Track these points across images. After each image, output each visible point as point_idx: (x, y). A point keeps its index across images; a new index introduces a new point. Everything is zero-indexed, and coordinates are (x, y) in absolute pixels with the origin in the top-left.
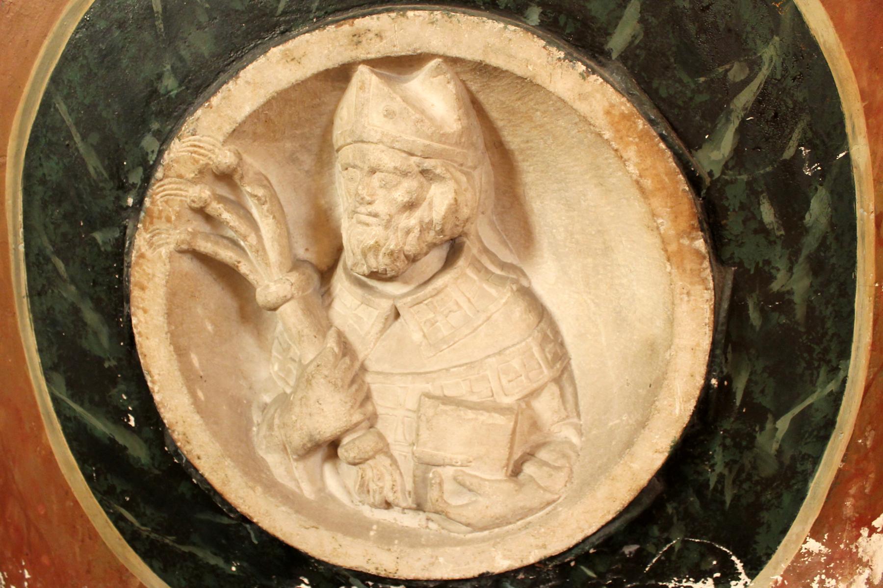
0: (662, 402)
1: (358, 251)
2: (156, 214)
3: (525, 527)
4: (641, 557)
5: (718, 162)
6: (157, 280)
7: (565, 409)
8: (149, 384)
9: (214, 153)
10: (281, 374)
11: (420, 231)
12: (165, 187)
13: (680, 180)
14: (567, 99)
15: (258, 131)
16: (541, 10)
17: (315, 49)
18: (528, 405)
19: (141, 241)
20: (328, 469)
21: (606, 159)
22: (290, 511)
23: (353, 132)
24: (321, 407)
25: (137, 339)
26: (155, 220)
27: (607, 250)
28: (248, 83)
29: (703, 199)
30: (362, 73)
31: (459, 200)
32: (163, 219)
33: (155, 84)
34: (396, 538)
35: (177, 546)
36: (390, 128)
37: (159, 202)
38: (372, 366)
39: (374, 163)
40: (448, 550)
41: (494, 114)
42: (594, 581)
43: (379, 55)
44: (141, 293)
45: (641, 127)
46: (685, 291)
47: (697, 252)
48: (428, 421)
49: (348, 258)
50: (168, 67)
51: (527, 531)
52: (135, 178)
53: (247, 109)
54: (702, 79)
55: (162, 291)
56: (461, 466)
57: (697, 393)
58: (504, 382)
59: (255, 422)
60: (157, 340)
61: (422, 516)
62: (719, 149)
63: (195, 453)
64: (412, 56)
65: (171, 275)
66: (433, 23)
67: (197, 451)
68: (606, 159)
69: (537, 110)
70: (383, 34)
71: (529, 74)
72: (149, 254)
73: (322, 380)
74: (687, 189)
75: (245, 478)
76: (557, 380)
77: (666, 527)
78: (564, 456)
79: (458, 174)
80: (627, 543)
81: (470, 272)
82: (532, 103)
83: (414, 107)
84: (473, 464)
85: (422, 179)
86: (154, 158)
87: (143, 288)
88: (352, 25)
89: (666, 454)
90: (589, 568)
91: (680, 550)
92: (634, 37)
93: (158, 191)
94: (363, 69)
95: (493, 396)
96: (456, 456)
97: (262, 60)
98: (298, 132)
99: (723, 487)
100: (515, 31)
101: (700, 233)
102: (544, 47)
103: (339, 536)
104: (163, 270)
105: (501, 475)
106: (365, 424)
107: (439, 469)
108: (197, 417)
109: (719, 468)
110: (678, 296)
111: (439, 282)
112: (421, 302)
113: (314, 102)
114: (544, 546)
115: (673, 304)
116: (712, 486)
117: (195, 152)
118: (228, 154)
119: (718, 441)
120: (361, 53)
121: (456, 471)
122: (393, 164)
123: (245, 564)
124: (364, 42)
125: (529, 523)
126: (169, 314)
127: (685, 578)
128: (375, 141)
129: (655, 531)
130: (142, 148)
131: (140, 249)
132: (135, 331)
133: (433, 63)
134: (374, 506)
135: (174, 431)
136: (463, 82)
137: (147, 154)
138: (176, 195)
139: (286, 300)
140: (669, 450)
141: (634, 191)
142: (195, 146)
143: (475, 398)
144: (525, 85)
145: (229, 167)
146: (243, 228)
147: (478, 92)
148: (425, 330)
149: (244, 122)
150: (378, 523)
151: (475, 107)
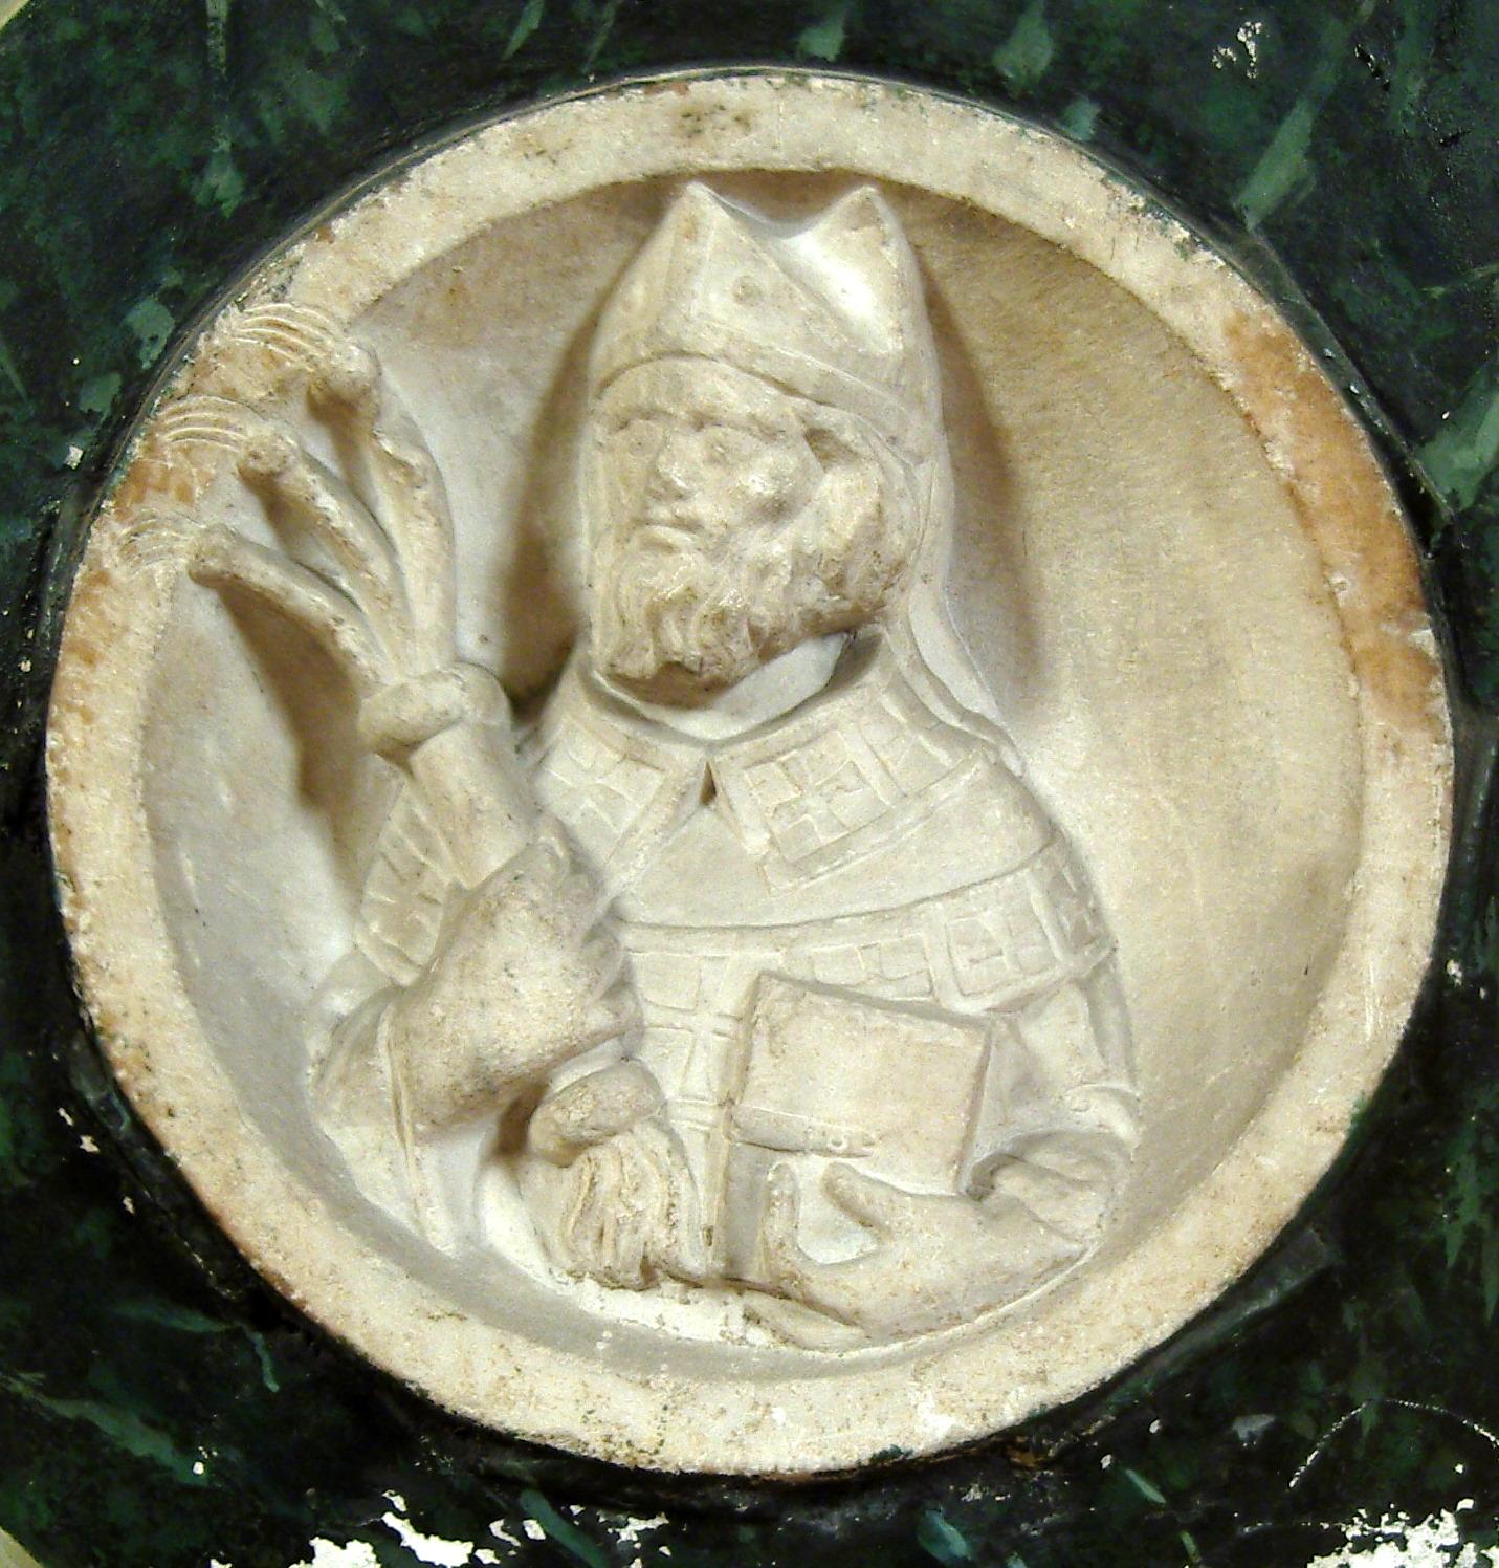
0: (1336, 1003)
1: (636, 615)
2: (156, 476)
3: (998, 1326)
4: (1279, 1450)
5: (1467, 474)
6: (131, 640)
7: (1103, 1054)
8: (66, 911)
9: (321, 348)
10: (389, 941)
11: (792, 573)
12: (189, 415)
13: (1384, 490)
14: (1145, 297)
15: (430, 312)
16: (1097, 110)
17: (598, 134)
18: (1013, 1027)
19: (106, 539)
20: (494, 1187)
21: (1226, 439)
22: (393, 1268)
23: (656, 331)
24: (513, 983)
25: (54, 787)
26: (150, 493)
27: (1216, 668)
28: (428, 194)
29: (1436, 555)
30: (693, 199)
31: (888, 511)
32: (172, 494)
33: (184, 182)
34: (665, 1361)
35: (46, 1402)
36: (747, 324)
37: (167, 452)
38: (639, 910)
39: (702, 400)
40: (800, 1387)
41: (976, 336)
42: (1159, 1515)
43: (739, 164)
44: (84, 670)
45: (1302, 368)
46: (1390, 742)
47: (1418, 654)
48: (772, 1034)
49: (599, 646)
50: (225, 145)
51: (1002, 1333)
52: (99, 398)
53: (419, 252)
54: (1438, 291)
55: (139, 671)
56: (849, 1154)
57: (1415, 987)
58: (961, 963)
59: (312, 1054)
60: (106, 793)
61: (736, 1306)
62: (1472, 444)
63: (161, 1099)
64: (811, 174)
65: (168, 635)
66: (864, 107)
67: (168, 1095)
68: (1226, 439)
69: (1075, 325)
70: (751, 120)
71: (1066, 237)
72: (120, 573)
73: (524, 915)
74: (1399, 512)
75: (287, 1174)
76: (1085, 985)
77: (1339, 1372)
78: (1101, 1161)
79: (886, 456)
80: (1242, 1411)
81: (887, 701)
82: (1065, 308)
83: (805, 287)
84: (876, 1151)
85: (807, 453)
86: (155, 354)
87: (90, 659)
88: (684, 91)
89: (1342, 1136)
90: (1147, 1475)
91: (1376, 1432)
92: (1298, 186)
93: (167, 422)
94: (699, 191)
95: (931, 992)
96: (835, 1127)
97: (468, 147)
98: (513, 334)
99: (1479, 1261)
100: (1043, 141)
101: (1426, 616)
102: (1103, 182)
103: (518, 1343)
104: (151, 617)
105: (942, 1186)
106: (610, 1046)
107: (792, 1162)
108: (181, 1003)
109: (1470, 1212)
110: (1373, 752)
111: (821, 714)
112: (771, 759)
113: (567, 263)
114: (1042, 1377)
115: (1362, 770)
116: (1451, 1261)
117: (276, 340)
118: (356, 352)
119: (1468, 1141)
120: (699, 156)
121: (834, 1165)
122: (748, 408)
123: (234, 1455)
124: (707, 133)
125: (1006, 1317)
126: (148, 731)
127: (1388, 1510)
128: (710, 351)
129: (1314, 1377)
130: (128, 329)
131: (99, 562)
132: (50, 767)
133: (856, 195)
134: (611, 1281)
135: (113, 1037)
136: (917, 249)
137: (139, 343)
138: (213, 437)
139: (446, 722)
140: (1348, 1125)
141: (1285, 514)
142: (279, 326)
143: (890, 993)
144: (1057, 260)
145: (354, 382)
146: (362, 540)
147: (944, 276)
148: (777, 830)
149: (405, 283)
150: (615, 1326)
151: (938, 314)
